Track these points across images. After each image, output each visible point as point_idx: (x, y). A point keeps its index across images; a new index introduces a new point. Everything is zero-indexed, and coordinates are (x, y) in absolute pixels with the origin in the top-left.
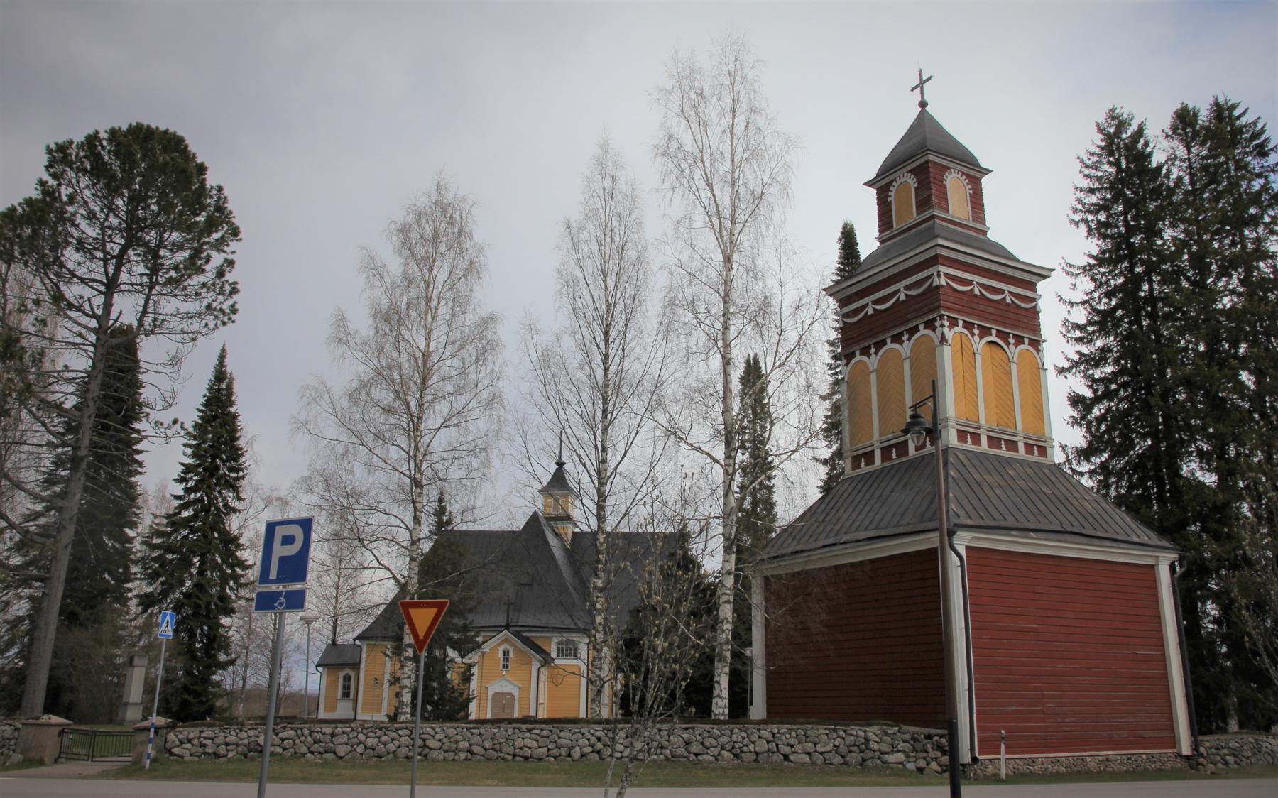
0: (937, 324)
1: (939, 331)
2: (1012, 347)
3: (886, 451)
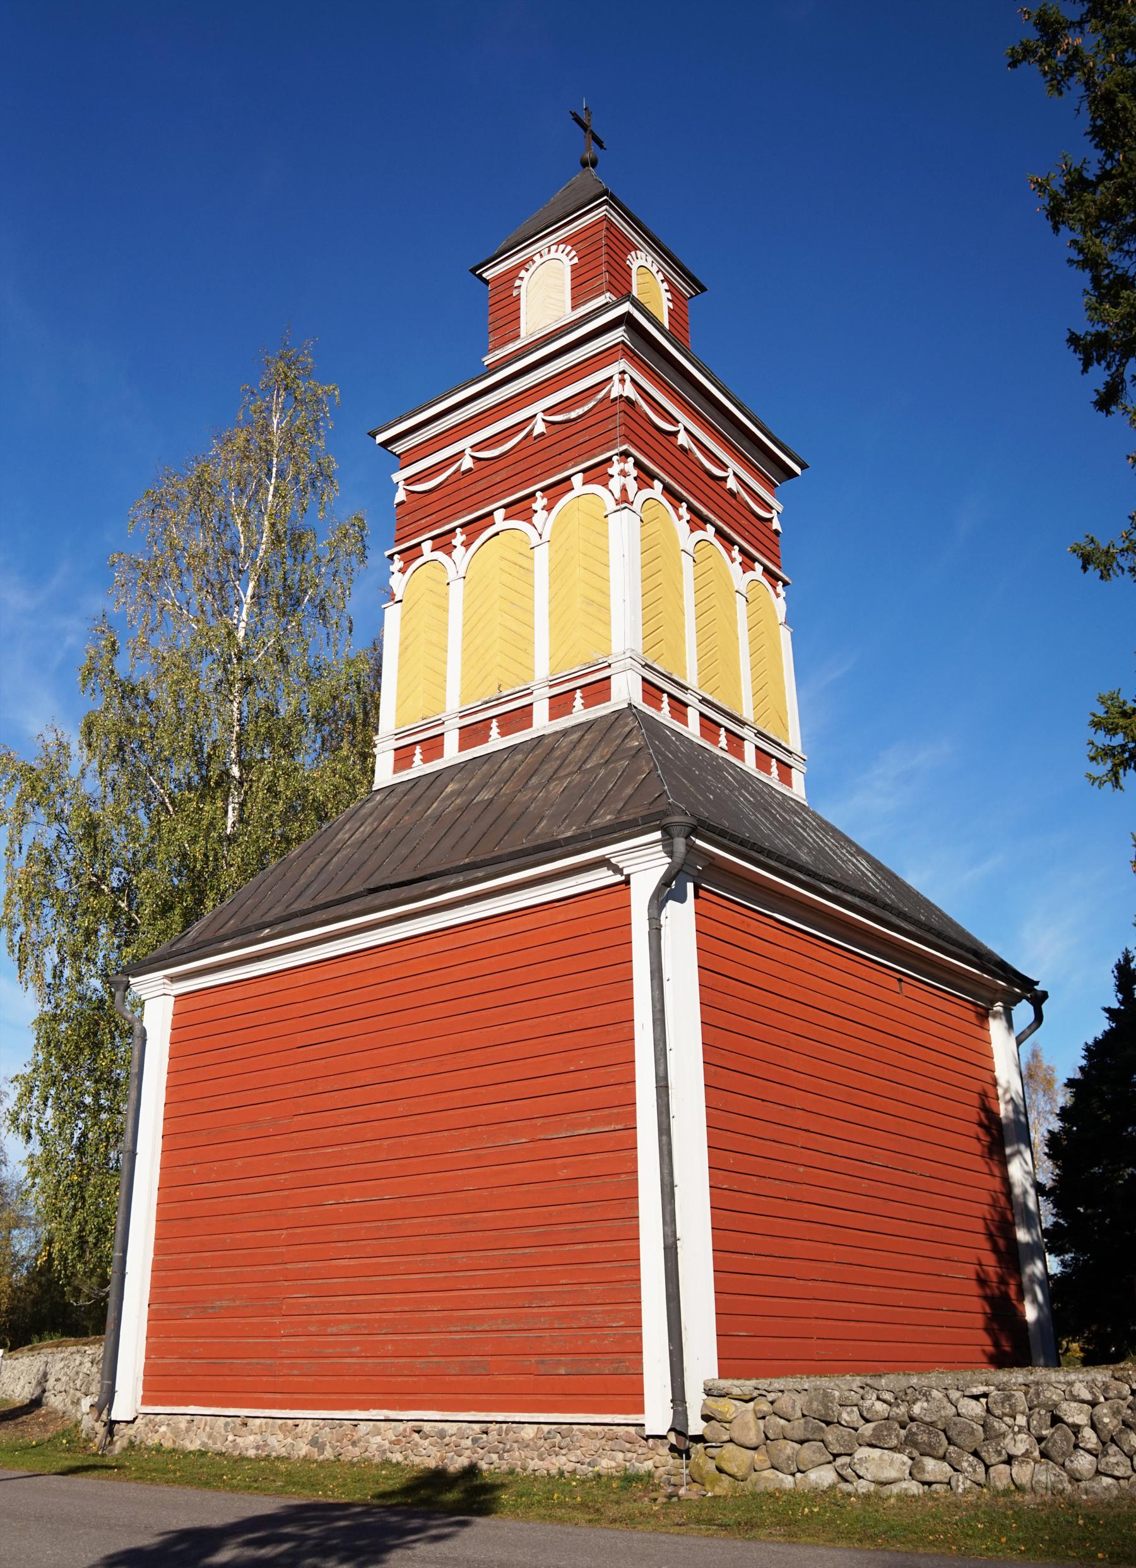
0: (614, 470)
1: (615, 484)
3: (560, 704)
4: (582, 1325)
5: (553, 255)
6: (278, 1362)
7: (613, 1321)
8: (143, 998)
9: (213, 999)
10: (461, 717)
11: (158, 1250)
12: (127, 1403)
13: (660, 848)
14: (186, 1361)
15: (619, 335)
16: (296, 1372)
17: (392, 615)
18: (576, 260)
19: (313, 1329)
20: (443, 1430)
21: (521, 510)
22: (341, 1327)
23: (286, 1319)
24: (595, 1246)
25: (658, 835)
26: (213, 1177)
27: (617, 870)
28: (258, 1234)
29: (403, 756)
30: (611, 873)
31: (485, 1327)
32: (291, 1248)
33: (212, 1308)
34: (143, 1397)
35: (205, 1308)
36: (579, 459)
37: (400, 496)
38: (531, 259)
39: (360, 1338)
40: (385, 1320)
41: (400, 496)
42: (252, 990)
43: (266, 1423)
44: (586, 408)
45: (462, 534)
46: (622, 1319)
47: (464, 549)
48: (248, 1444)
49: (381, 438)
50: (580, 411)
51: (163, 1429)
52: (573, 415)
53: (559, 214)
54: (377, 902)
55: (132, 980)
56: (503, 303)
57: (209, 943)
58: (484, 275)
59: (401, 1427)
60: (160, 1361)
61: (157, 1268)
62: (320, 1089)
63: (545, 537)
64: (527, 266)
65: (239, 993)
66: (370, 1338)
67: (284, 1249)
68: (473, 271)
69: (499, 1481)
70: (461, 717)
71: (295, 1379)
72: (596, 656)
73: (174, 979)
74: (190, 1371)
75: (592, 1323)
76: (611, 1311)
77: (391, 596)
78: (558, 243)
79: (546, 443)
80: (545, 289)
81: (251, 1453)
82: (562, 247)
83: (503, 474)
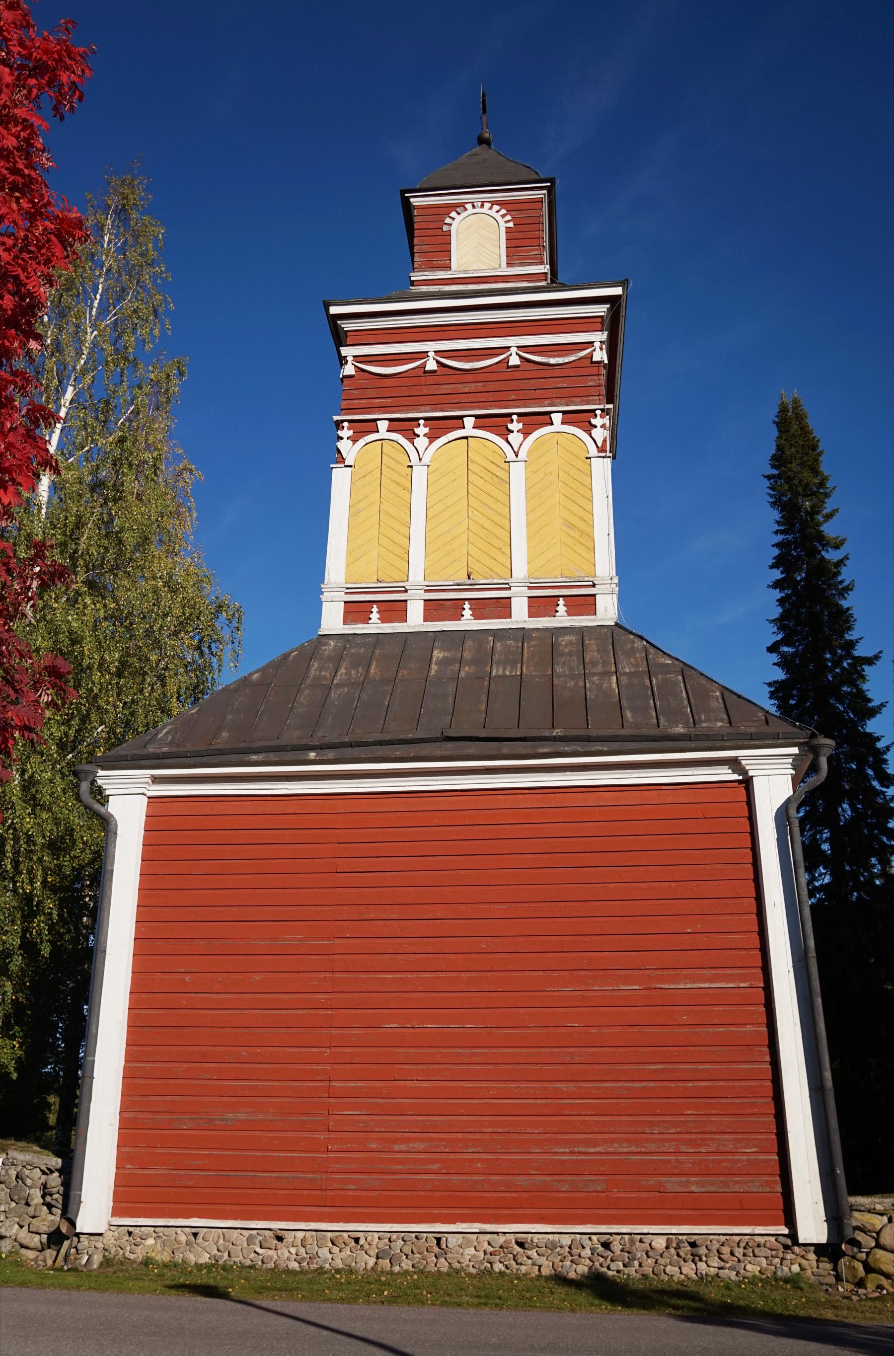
2: (515, 438)
3: (541, 605)
4: (711, 1150)
5: (492, 212)
6: (324, 1176)
7: (745, 1148)
8: (107, 792)
9: (206, 808)
10: (426, 591)
11: (130, 1058)
12: (95, 1210)
13: (791, 761)
14: (183, 1172)
15: (601, 310)
16: (352, 1187)
17: (340, 478)
18: (511, 225)
19: (373, 1146)
20: (552, 1242)
21: (497, 425)
22: (411, 1145)
23: (333, 1135)
24: (721, 1083)
25: (795, 750)
26: (216, 988)
27: (743, 771)
28: (289, 1050)
29: (355, 611)
30: (730, 771)
31: (599, 1149)
32: (336, 1066)
33: (222, 1120)
34: (113, 1208)
35: (211, 1120)
36: (557, 401)
37: (349, 370)
38: (462, 205)
39: (438, 1156)
40: (470, 1140)
41: (349, 370)
42: (269, 807)
43: (312, 1236)
44: (566, 360)
45: (425, 426)
46: (755, 1146)
47: (427, 440)
48: (286, 1256)
49: (334, 310)
50: (560, 360)
51: (150, 1241)
52: (553, 361)
53: (503, 180)
54: (471, 751)
55: (101, 773)
56: (431, 232)
57: (222, 752)
58: (412, 200)
59: (501, 1239)
60: (140, 1172)
61: (128, 1075)
62: (373, 916)
63: (522, 455)
64: (458, 210)
65: (248, 808)
66: (452, 1156)
67: (328, 1067)
68: (403, 192)
69: (173, 1292)
70: (426, 591)
71: (351, 1193)
72: (577, 574)
73: (156, 780)
74: (190, 1183)
75: (722, 1148)
76: (744, 1139)
77: (340, 459)
78: (493, 203)
79: (519, 375)
80: (478, 236)
81: (294, 1265)
82: (496, 208)
83: (472, 387)
